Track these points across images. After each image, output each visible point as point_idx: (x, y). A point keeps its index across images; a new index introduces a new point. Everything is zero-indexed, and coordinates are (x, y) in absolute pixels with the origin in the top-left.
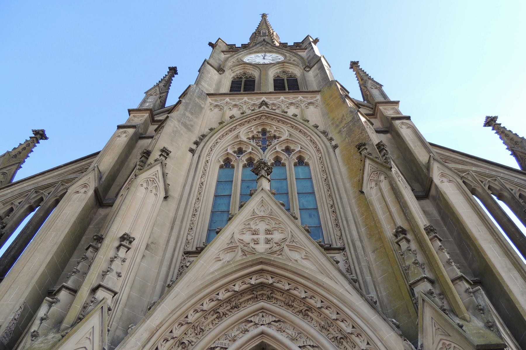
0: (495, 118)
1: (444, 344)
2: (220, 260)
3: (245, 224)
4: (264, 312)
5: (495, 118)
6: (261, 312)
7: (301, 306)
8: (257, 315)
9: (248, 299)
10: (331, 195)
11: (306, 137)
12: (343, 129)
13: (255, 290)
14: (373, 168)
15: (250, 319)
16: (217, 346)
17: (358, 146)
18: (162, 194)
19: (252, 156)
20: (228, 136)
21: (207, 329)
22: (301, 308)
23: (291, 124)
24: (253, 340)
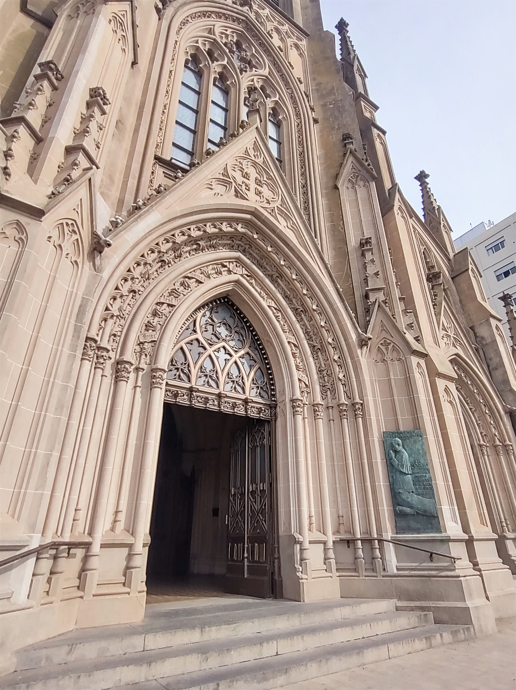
0: (427, 176)
1: (385, 341)
2: (212, 189)
3: (237, 160)
4: (239, 263)
5: (427, 176)
6: (236, 262)
7: (273, 270)
8: (232, 262)
9: (226, 244)
10: (305, 173)
11: (287, 87)
12: (330, 105)
13: (235, 237)
14: (354, 168)
15: (225, 264)
16: (193, 277)
17: (346, 135)
18: (131, 58)
19: (225, 72)
20: (200, 20)
21: (184, 256)
22: (273, 273)
23: (274, 58)
24: (227, 285)
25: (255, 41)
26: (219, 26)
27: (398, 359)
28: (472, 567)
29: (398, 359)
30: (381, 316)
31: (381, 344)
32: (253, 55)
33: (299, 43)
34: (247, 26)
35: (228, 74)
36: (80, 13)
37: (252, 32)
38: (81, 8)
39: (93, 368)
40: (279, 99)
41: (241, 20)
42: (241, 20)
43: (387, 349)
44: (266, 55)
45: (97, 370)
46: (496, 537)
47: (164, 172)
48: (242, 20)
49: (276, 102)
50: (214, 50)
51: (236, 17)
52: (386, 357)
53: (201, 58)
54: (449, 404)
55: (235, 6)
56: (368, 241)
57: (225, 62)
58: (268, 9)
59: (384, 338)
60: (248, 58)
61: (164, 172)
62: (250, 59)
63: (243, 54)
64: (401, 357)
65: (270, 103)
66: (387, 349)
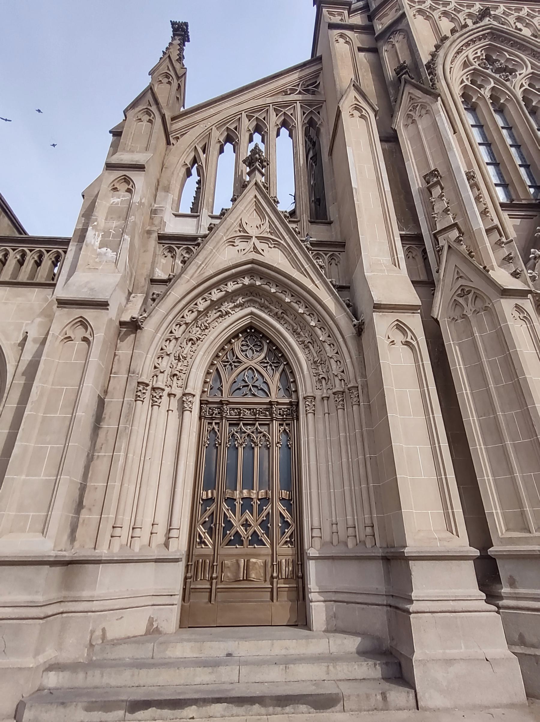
23: (532, 49)
25: (506, 45)
26: (470, 53)
27: (484, 309)
28: (485, 598)
29: (484, 309)
30: (454, 261)
31: (459, 296)
32: (508, 60)
33: (521, 14)
34: (493, 36)
35: (497, 94)
36: (416, 119)
37: (499, 38)
38: (413, 114)
39: (150, 406)
40: (495, 83)
41: (486, 35)
42: (486, 35)
43: (466, 300)
44: (522, 52)
45: (154, 407)
46: (476, 553)
47: (508, 215)
48: (488, 33)
49: (493, 89)
50: (475, 79)
51: (482, 35)
52: (465, 311)
53: (470, 94)
54: (406, 347)
55: (478, 25)
56: (434, 173)
57: (493, 84)
58: (525, 7)
59: (461, 286)
60: (503, 66)
61: (508, 215)
62: (505, 66)
63: (497, 65)
64: (487, 305)
65: (486, 92)
66: (466, 300)
